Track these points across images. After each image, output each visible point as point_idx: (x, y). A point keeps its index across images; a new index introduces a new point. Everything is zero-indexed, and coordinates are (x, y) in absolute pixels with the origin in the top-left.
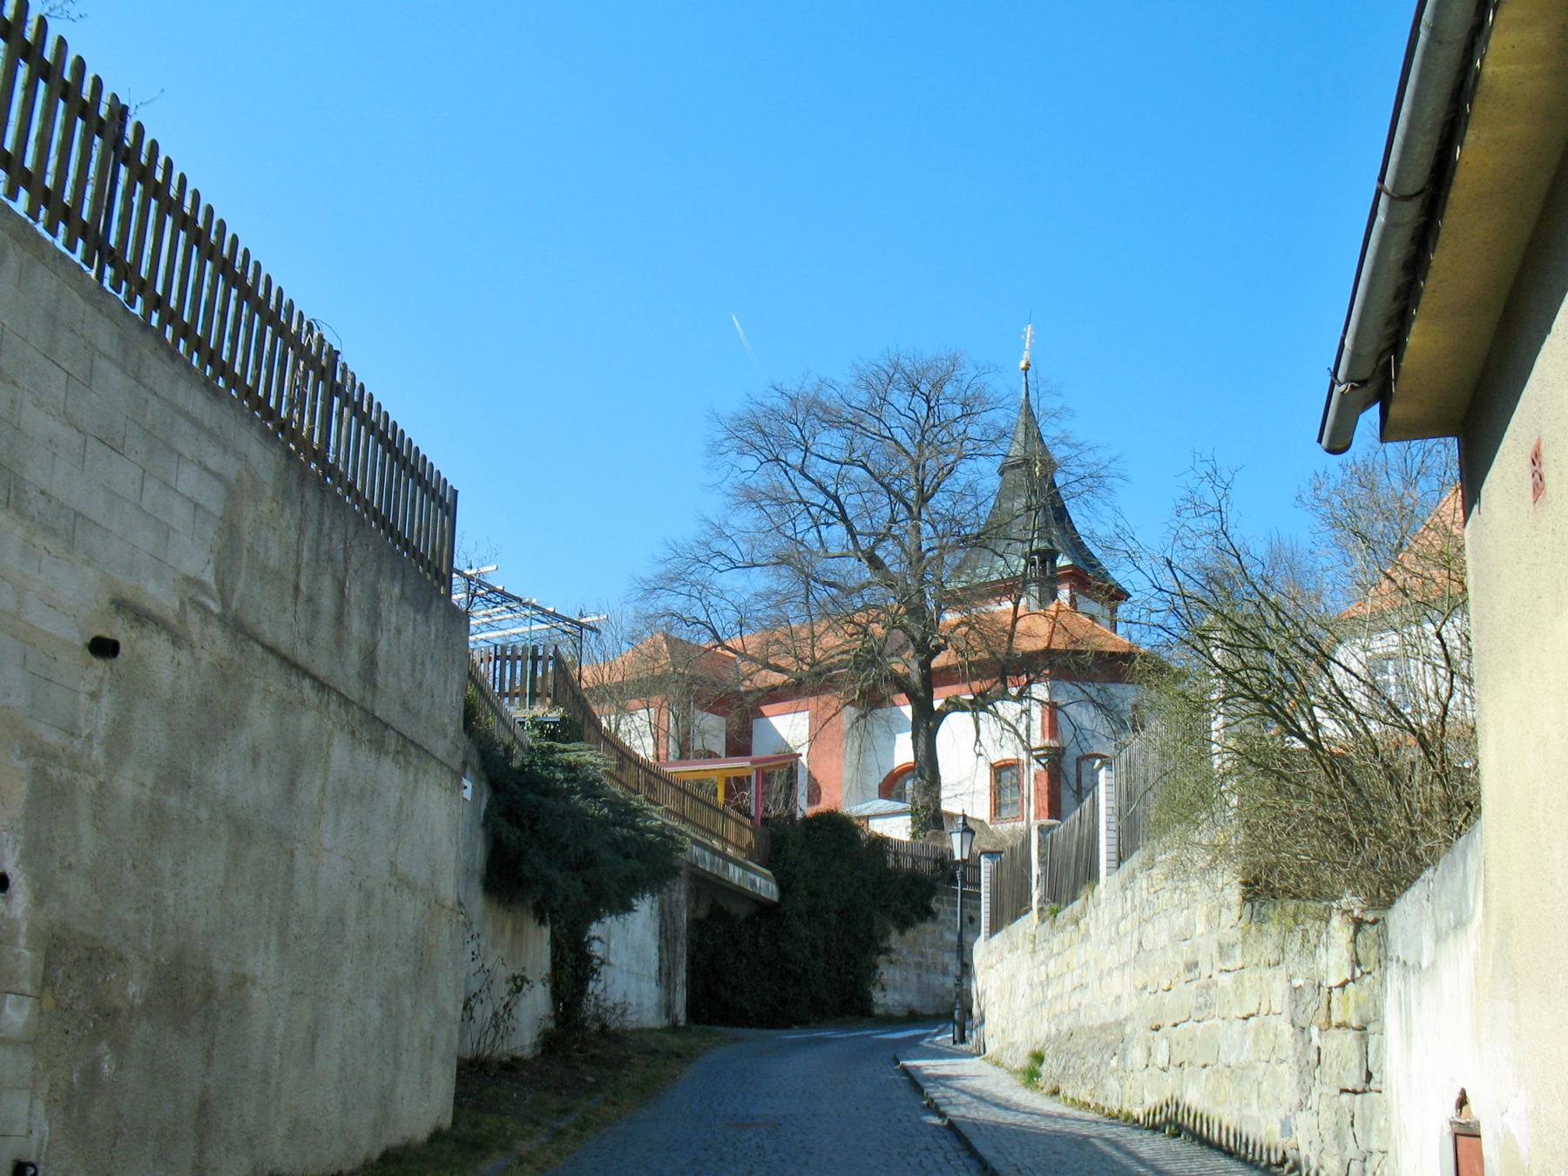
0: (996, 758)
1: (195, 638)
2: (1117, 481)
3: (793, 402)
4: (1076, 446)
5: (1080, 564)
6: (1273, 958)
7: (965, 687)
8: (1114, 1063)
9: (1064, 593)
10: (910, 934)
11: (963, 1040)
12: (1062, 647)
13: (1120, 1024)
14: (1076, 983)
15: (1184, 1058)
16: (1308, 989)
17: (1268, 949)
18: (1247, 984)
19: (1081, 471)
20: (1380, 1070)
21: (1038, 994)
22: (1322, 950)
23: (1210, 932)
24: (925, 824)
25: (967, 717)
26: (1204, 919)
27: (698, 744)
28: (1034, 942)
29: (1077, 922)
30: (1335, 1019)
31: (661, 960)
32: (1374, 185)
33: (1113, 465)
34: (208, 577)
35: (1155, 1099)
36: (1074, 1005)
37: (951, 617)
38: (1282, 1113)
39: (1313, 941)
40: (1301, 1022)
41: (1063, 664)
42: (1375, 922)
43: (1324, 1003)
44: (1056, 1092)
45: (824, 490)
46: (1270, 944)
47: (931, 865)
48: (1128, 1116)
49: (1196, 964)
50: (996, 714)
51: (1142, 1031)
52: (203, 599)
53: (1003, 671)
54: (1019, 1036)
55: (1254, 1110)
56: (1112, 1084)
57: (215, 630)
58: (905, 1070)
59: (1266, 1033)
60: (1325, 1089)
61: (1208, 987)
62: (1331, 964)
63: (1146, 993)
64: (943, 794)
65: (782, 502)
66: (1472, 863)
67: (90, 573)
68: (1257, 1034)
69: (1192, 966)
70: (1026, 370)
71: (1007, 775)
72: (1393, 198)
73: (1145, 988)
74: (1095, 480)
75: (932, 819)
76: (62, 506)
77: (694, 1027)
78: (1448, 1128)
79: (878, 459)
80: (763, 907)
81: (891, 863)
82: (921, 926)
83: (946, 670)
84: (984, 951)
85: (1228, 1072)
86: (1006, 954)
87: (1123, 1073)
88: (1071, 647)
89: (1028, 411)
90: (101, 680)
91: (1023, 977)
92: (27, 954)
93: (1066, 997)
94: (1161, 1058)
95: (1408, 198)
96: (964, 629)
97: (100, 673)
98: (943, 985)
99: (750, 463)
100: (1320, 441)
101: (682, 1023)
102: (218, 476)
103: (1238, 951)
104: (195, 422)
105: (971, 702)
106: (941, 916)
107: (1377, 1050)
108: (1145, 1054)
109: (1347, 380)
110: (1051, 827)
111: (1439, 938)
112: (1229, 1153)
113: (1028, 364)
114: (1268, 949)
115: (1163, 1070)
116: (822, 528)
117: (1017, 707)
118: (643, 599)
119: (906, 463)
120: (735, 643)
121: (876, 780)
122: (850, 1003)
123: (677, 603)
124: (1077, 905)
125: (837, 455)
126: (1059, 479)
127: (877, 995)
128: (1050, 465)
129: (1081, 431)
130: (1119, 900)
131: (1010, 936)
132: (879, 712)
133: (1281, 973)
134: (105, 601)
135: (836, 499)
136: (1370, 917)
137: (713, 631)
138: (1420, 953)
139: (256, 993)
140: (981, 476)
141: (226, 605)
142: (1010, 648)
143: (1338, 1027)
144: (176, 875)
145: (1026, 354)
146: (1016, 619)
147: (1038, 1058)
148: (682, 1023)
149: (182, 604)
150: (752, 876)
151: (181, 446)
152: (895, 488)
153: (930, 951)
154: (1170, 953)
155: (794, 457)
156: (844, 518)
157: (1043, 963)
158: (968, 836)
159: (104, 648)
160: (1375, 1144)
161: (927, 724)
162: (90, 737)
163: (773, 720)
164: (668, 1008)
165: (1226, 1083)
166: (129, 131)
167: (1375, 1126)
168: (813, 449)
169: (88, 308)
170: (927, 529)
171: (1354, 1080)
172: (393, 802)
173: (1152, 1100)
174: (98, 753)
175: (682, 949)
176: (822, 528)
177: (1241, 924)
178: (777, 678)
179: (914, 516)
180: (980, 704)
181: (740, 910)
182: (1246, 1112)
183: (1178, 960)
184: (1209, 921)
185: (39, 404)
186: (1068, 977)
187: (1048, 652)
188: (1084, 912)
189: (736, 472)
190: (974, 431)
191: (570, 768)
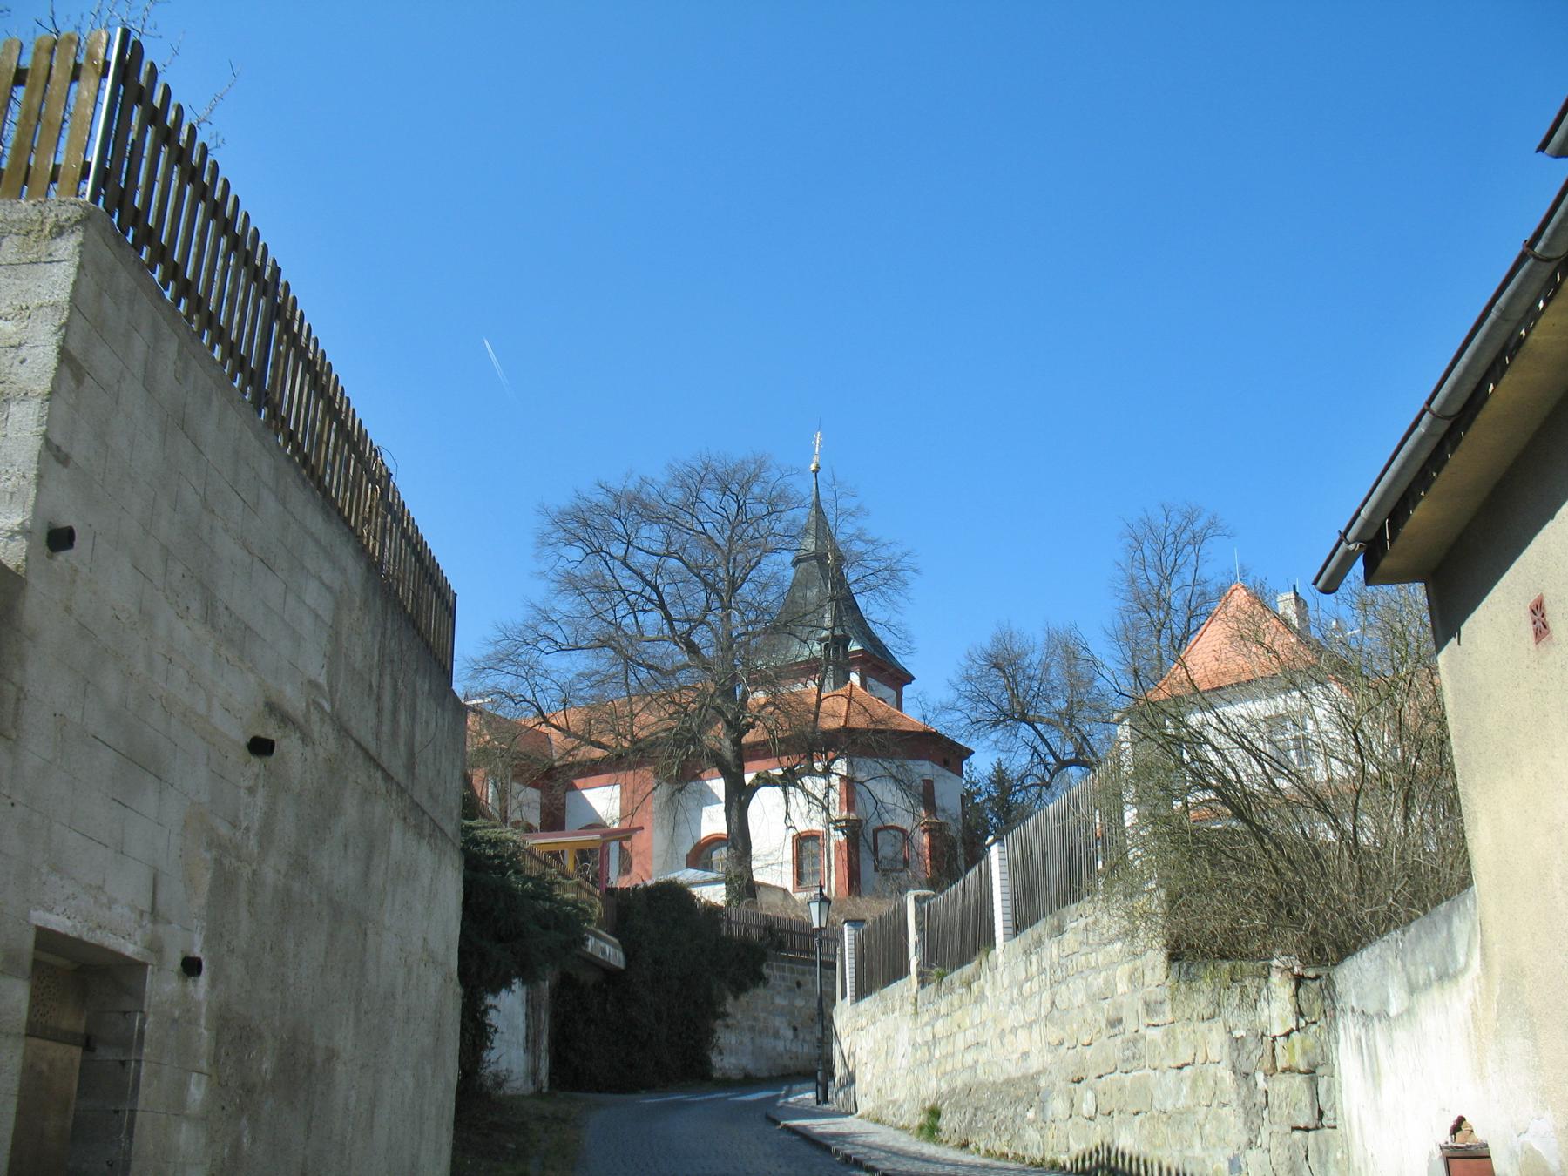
0: (802, 827)
1: (316, 735)
2: (908, 573)
3: (617, 498)
4: (872, 542)
6: (1210, 1010)
8: (1031, 1114)
9: (855, 678)
10: (744, 999)
11: (826, 1100)
13: (1034, 1078)
14: (970, 1039)
16: (1250, 1039)
17: (1202, 1003)
18: (1179, 1036)
19: (876, 564)
21: (922, 1054)
22: (1263, 1003)
23: (1134, 991)
24: (739, 893)
25: (777, 792)
26: (1125, 979)
27: (516, 816)
28: (915, 1004)
29: (969, 985)
30: (1279, 1066)
32: (1421, 404)
33: (906, 559)
34: (322, 680)
37: (760, 696)
38: (1229, 1153)
39: (1253, 995)
40: (1245, 1068)
41: (848, 741)
42: (1317, 977)
43: (1269, 1052)
44: (965, 1145)
45: (643, 579)
46: (1203, 1000)
48: (1054, 1165)
50: (803, 789)
53: (804, 748)
54: (900, 1094)
55: (1198, 1150)
56: (1031, 1135)
57: (328, 728)
58: (793, 1131)
59: (1205, 1080)
60: (1276, 1128)
61: (1135, 1042)
62: (1274, 1015)
63: (1063, 1049)
64: (754, 865)
65: (605, 590)
66: (1460, 926)
67: (252, 678)
68: (1194, 1081)
69: (1115, 1022)
70: (816, 472)
71: (810, 845)
73: (1061, 1043)
74: (890, 576)
75: (744, 887)
76: (238, 620)
77: (560, 1095)
78: (1438, 1153)
79: (695, 553)
80: (609, 972)
81: (725, 931)
83: (754, 745)
84: (844, 1015)
85: (1164, 1117)
86: (879, 1015)
87: (1043, 1123)
88: (872, 726)
90: (258, 776)
91: (903, 1037)
92: (206, 1033)
94: (1087, 1107)
95: (1445, 418)
97: (256, 770)
98: (774, 1048)
99: (575, 553)
102: (329, 589)
103: (1167, 1007)
106: (772, 981)
107: (1329, 1090)
108: (1068, 1104)
109: (1356, 540)
110: (926, 898)
111: (1412, 989)
113: (818, 467)
114: (1202, 1003)
115: (1090, 1119)
116: (640, 615)
117: (822, 782)
118: (472, 678)
119: (719, 558)
121: (687, 848)
122: (690, 1066)
123: (505, 682)
124: (968, 969)
125: (655, 547)
126: (851, 576)
127: (715, 1059)
129: (875, 523)
132: (693, 785)
134: (261, 704)
135: (655, 588)
136: (1311, 973)
137: (539, 709)
138: (1385, 1002)
139: (340, 1067)
140: (780, 567)
143: (1283, 1071)
144: (295, 956)
145: (816, 458)
146: (819, 701)
147: (935, 1113)
149: (308, 705)
150: (602, 944)
152: (711, 579)
153: (762, 1015)
154: (1089, 1012)
156: (662, 606)
157: (927, 1024)
159: (260, 747)
161: (739, 799)
162: (247, 829)
164: (534, 1073)
165: (1163, 1128)
166: (281, 290)
167: (1331, 1158)
168: (635, 543)
173: (1078, 1148)
174: (253, 842)
175: (544, 1017)
176: (640, 615)
177: (1168, 983)
178: (598, 753)
179: (726, 607)
180: (789, 780)
181: (589, 977)
182: (1188, 1153)
183: (1099, 1017)
184: (1131, 980)
185: (227, 530)
187: (848, 731)
189: (563, 562)
190: (779, 528)
191: (494, 844)
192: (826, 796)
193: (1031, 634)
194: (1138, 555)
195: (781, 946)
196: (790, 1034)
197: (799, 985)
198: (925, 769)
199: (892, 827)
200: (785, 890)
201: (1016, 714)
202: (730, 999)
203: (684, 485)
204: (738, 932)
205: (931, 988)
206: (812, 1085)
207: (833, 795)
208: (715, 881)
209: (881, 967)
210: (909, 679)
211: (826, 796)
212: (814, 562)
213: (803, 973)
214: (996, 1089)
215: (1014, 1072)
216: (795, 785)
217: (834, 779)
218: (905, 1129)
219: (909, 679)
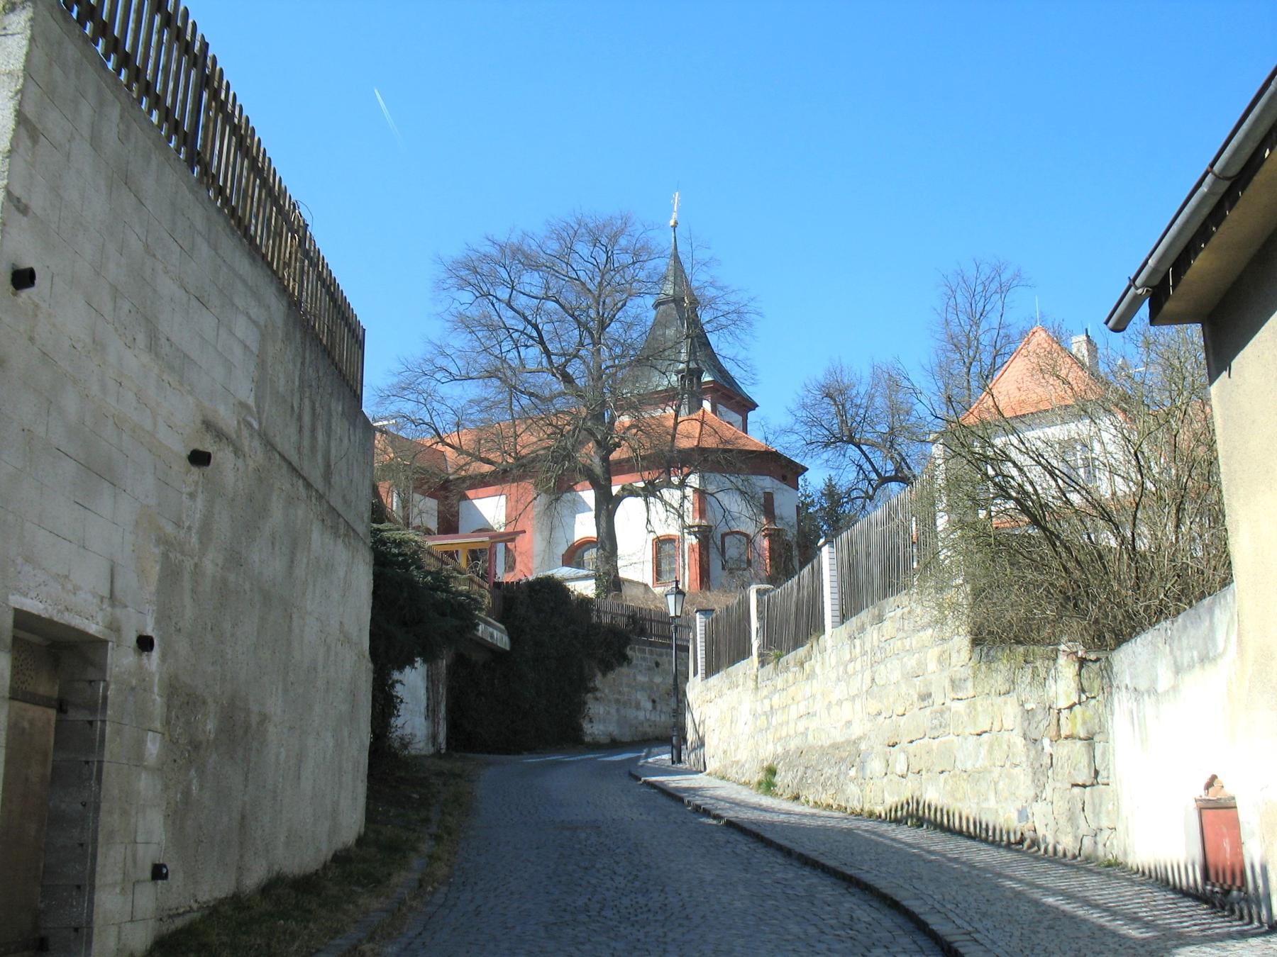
0: (662, 531)
1: (246, 449)
4: (722, 289)
5: (721, 381)
7: (636, 476)
8: (853, 772)
9: (707, 405)
10: (611, 676)
11: (680, 761)
12: (714, 446)
15: (922, 766)
16: (1039, 711)
18: (980, 709)
19: (726, 308)
20: (1107, 768)
21: (762, 721)
22: (1050, 682)
23: (942, 670)
24: (607, 587)
29: (802, 665)
30: (1063, 733)
31: (428, 699)
34: (251, 402)
35: (896, 799)
36: (801, 728)
37: (626, 420)
42: (1098, 660)
43: (1054, 721)
45: (525, 318)
46: (1000, 678)
47: (624, 620)
48: (871, 814)
49: (930, 695)
50: (661, 499)
51: (879, 748)
52: (249, 419)
53: (664, 463)
54: (743, 755)
56: (852, 789)
57: (256, 443)
58: (652, 785)
60: (1058, 785)
61: (942, 713)
62: (1060, 691)
63: (881, 718)
64: (620, 563)
65: (492, 328)
67: (191, 400)
70: (674, 227)
71: (667, 547)
72: (1217, 177)
73: (879, 714)
74: (738, 317)
75: (611, 583)
79: (570, 297)
81: (595, 619)
82: (618, 670)
83: (619, 462)
84: (696, 689)
85: (965, 776)
86: (725, 691)
87: (862, 780)
88: (721, 446)
89: (676, 257)
92: (158, 698)
93: (792, 725)
94: (900, 767)
96: (634, 431)
97: (196, 478)
98: (636, 718)
99: (467, 296)
100: (1106, 323)
101: (443, 751)
103: (969, 684)
104: (244, 282)
105: (643, 489)
106: (634, 662)
107: (1104, 754)
108: (884, 764)
109: (1143, 285)
110: (766, 591)
111: (1178, 670)
112: (970, 837)
113: (676, 223)
120: (454, 440)
121: (562, 549)
122: (567, 735)
123: (408, 407)
124: (801, 652)
125: (535, 291)
127: (586, 726)
128: (695, 303)
129: (724, 272)
130: (847, 648)
131: (729, 676)
133: (1012, 700)
135: (536, 327)
136: (1093, 656)
137: (436, 430)
139: (271, 729)
140: (643, 309)
141: (260, 424)
142: (673, 446)
144: (232, 635)
145: (674, 215)
146: (676, 424)
148: (443, 751)
149: (239, 422)
150: (491, 629)
151: (237, 301)
153: (626, 690)
155: (503, 293)
156: (542, 342)
158: (680, 597)
159: (199, 458)
160: (1105, 823)
161: (607, 506)
162: (189, 528)
163: (475, 502)
164: (434, 737)
166: (209, 62)
167: (1104, 808)
168: (517, 287)
169: (190, 196)
170: (605, 352)
171: (1083, 776)
172: (341, 574)
173: (891, 800)
177: (971, 664)
178: (487, 468)
180: (650, 491)
182: (985, 805)
183: (912, 692)
186: (794, 708)
187: (701, 450)
188: (809, 657)
189: (456, 304)
190: (642, 275)
192: (681, 505)
193: (860, 373)
194: (952, 302)
195: (642, 631)
196: (649, 705)
197: (657, 664)
198: (766, 483)
199: (738, 533)
200: (646, 585)
201: (845, 437)
202: (599, 676)
203: (560, 237)
204: (606, 620)
205: (770, 667)
206: (668, 748)
207: (687, 505)
208: (586, 577)
209: (727, 649)
210: (754, 406)
211: (681, 505)
212: (673, 305)
213: (661, 655)
214: (823, 751)
215: (839, 737)
216: (655, 496)
217: (689, 491)
218: (747, 784)
219: (754, 406)
